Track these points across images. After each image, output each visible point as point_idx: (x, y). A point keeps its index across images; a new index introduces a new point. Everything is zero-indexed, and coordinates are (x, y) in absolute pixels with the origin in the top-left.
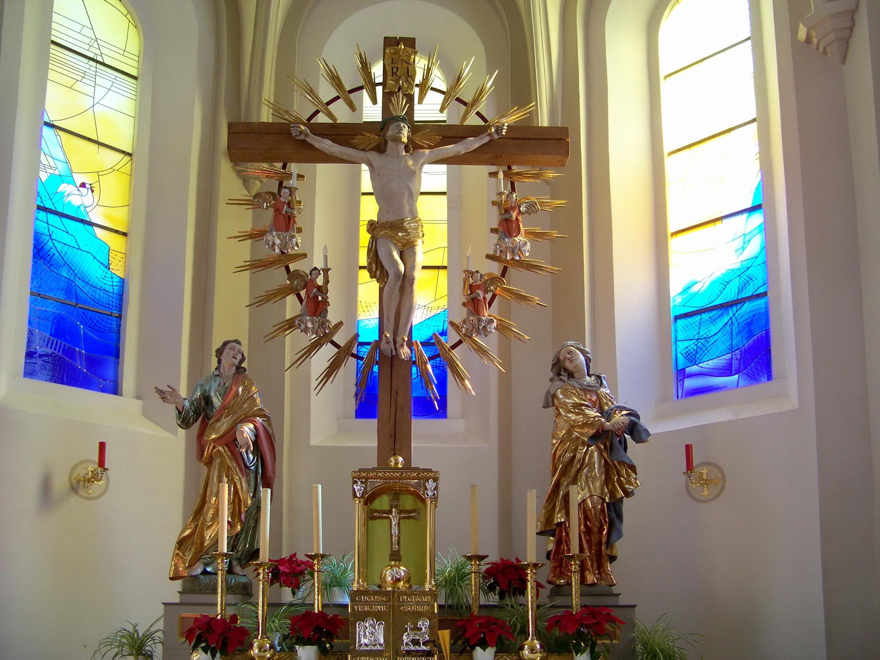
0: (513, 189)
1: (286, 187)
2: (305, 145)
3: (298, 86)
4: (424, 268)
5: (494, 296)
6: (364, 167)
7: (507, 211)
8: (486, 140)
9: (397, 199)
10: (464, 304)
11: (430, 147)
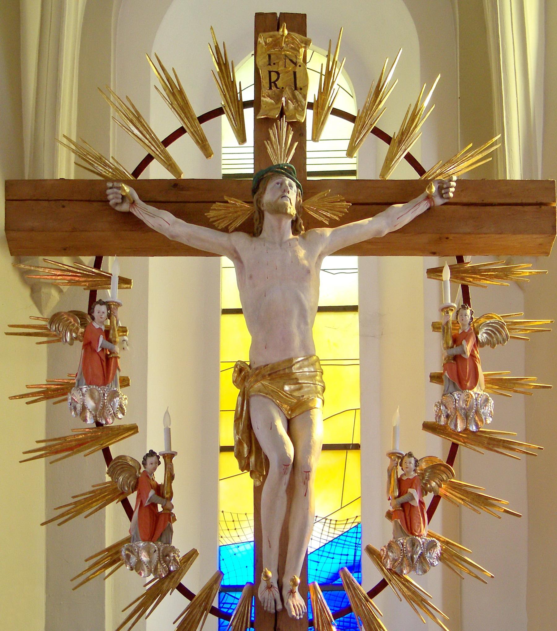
0: (466, 299)
1: (101, 303)
2: (131, 221)
3: (117, 109)
4: (326, 447)
5: (437, 499)
6: (226, 261)
7: (456, 341)
8: (423, 207)
9: (277, 313)
10: (389, 515)
11: (333, 224)
